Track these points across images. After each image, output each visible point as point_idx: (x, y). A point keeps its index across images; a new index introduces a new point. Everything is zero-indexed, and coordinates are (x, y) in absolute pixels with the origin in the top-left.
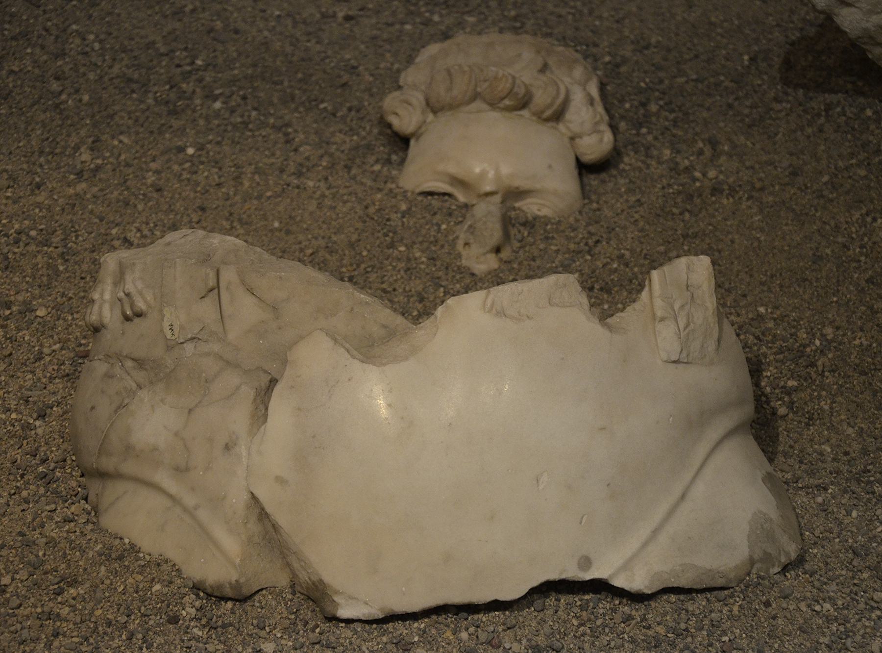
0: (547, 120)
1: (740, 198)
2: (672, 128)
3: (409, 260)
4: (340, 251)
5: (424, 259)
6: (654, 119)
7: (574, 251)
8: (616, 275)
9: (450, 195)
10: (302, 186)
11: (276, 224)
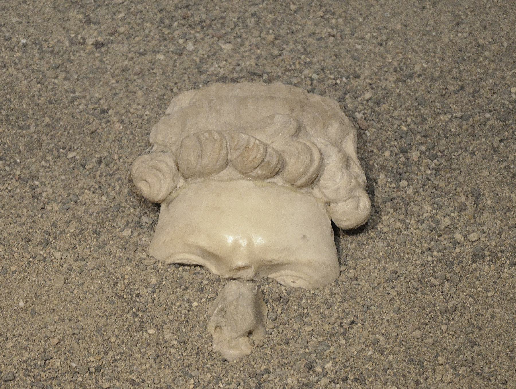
0: (301, 187)
1: (502, 265)
2: (433, 178)
3: (159, 344)
4: (87, 338)
5: (174, 342)
6: (415, 168)
7: (328, 333)
8: (371, 363)
10: (49, 259)
11: (22, 304)
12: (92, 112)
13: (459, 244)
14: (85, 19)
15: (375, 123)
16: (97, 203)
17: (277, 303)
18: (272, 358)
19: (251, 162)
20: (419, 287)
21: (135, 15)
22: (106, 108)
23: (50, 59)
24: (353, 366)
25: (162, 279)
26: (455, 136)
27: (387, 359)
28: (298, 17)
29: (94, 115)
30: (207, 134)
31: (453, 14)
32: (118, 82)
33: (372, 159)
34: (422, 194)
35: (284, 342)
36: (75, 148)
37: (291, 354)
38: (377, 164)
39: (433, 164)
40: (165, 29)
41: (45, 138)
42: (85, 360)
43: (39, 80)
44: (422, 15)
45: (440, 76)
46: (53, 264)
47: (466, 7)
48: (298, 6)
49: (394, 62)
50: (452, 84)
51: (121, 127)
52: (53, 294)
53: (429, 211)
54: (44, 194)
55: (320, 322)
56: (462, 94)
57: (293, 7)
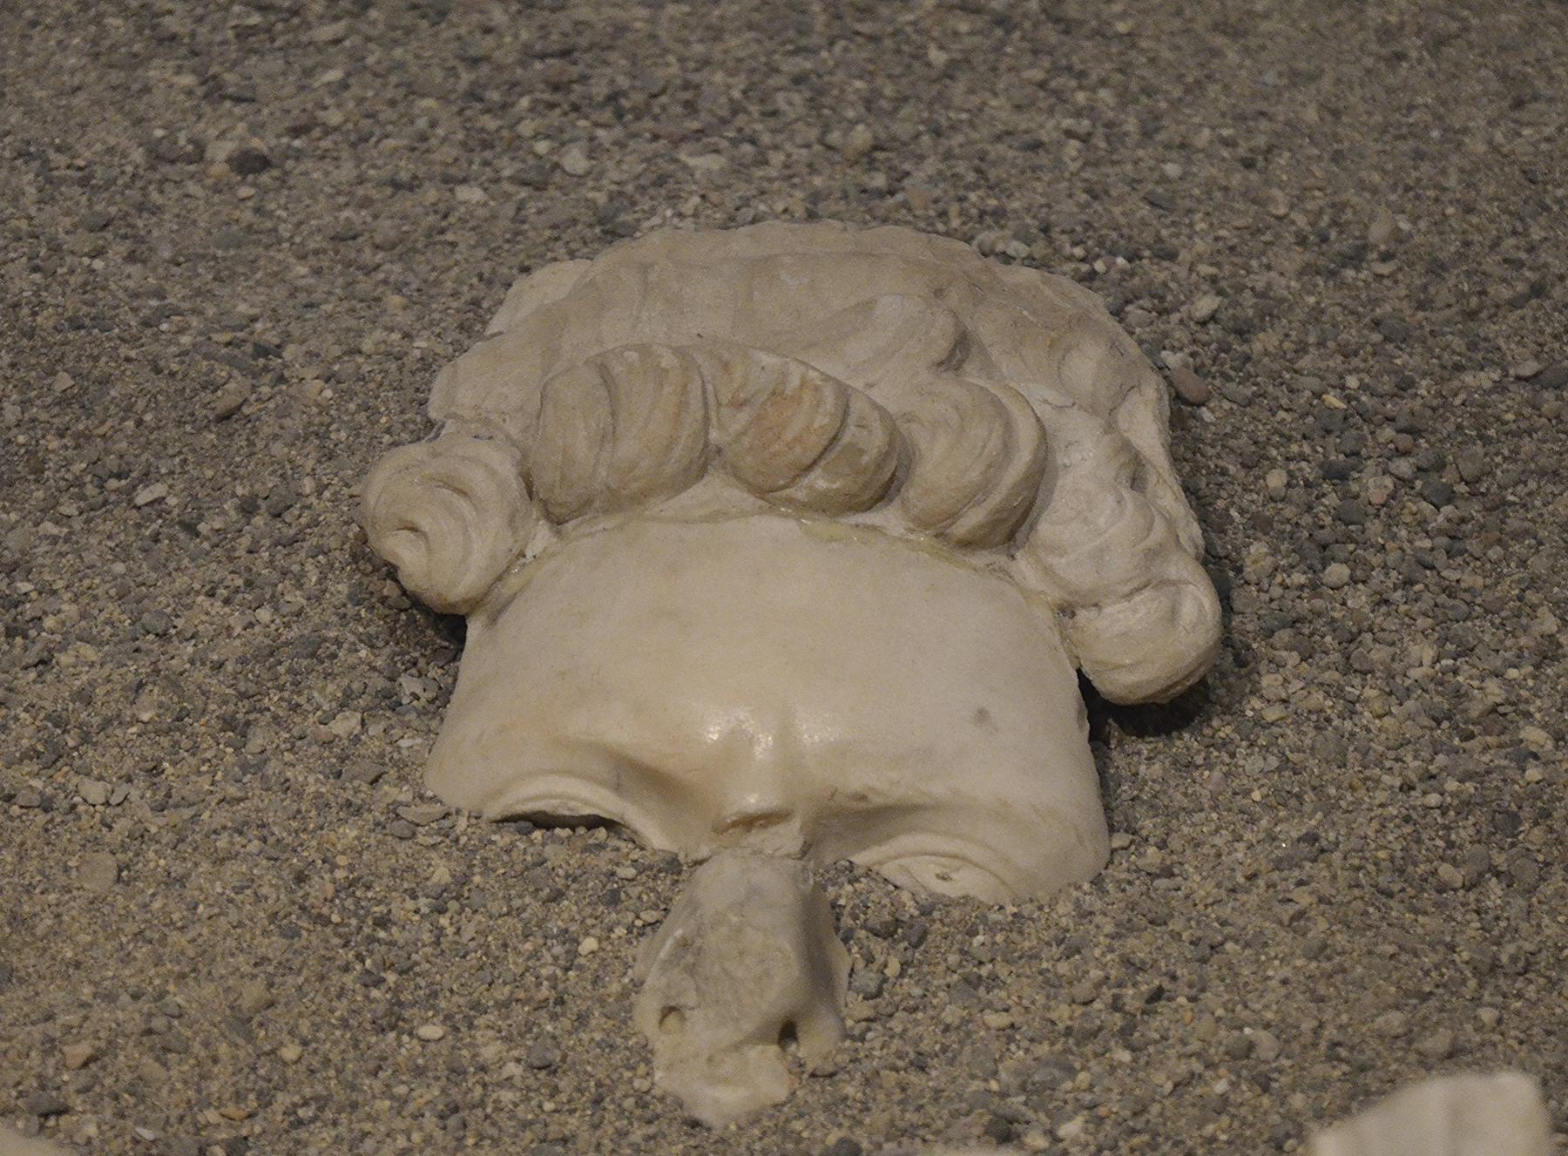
0: (969, 544)
3: (456, 1071)
4: (197, 1047)
5: (513, 1069)
6: (1374, 528)
7: (1069, 1031)
8: (1225, 1120)
9: (610, 825)
10: (62, 803)
12: (224, 351)
13: (1536, 756)
14: (204, 88)
15: (1232, 386)
16: (238, 630)
17: (885, 944)
18: (868, 1109)
19: (790, 446)
20: (1396, 888)
21: (383, 76)
22: (277, 341)
23: (77, 203)
24: (1161, 1130)
25: (470, 867)
26: (1518, 434)
27: (1282, 1104)
28: (958, 89)
29: (231, 361)
30: (635, 355)
31: (1503, 76)
32: (317, 272)
33: (1223, 494)
34: (1403, 608)
35: (912, 1063)
36: (163, 471)
37: (936, 1100)
38: (1242, 512)
39: (1440, 518)
40: (487, 117)
41: (54, 444)
42: (188, 1119)
43: (38, 262)
44: (1391, 80)
45: (1461, 257)
46: (79, 818)
47: (1549, 52)
48: (958, 56)
49: (1293, 215)
50: (1504, 280)
51: (328, 393)
52: (74, 913)
53: (1427, 661)
54: (49, 622)
55: (1040, 999)
56: (1541, 307)
57: (937, 56)
